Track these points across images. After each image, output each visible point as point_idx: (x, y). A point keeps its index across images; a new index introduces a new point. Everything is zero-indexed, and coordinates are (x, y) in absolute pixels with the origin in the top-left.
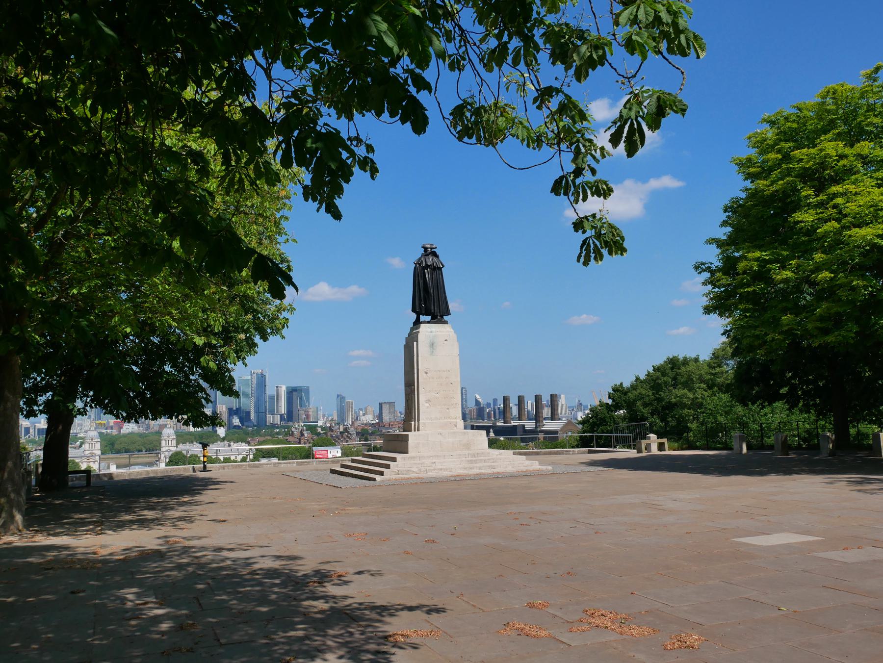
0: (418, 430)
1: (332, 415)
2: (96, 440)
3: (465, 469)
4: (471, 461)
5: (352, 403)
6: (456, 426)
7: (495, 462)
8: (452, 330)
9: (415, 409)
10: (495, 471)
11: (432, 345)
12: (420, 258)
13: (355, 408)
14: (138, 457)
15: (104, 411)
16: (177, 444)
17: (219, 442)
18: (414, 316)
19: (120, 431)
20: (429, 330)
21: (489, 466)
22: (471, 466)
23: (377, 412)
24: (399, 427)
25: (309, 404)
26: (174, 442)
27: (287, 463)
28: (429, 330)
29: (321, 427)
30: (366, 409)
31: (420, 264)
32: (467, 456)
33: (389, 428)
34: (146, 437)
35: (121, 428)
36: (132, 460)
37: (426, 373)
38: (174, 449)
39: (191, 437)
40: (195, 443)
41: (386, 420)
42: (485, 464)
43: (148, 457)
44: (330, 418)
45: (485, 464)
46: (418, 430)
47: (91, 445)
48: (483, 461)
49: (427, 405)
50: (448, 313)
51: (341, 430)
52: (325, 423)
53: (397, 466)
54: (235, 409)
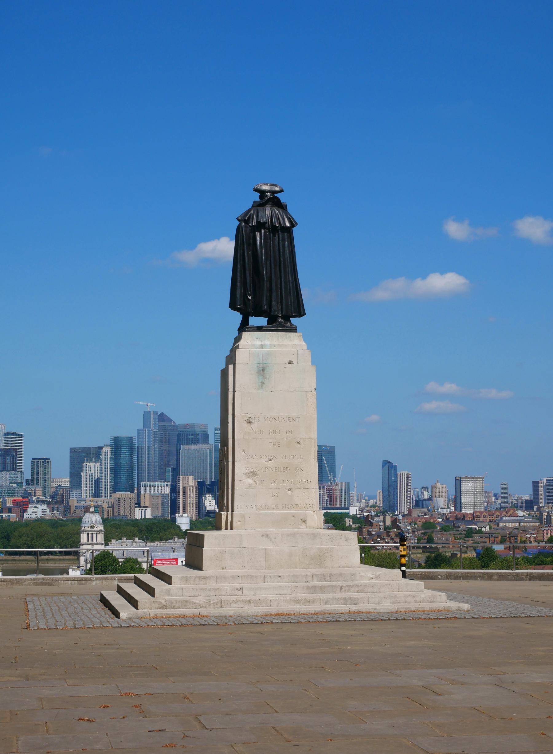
0: (232, 528)
1: (375, 497)
2: (98, 529)
3: (297, 602)
4: (314, 587)
5: (408, 478)
6: (304, 522)
7: (362, 591)
8: (304, 343)
9: (228, 489)
10: (354, 608)
11: (262, 371)
12: (249, 210)
13: (416, 485)
14: (47, 560)
15: (197, 486)
16: (107, 542)
17: (176, 539)
18: (238, 317)
19: (22, 516)
20: (258, 343)
21: (345, 599)
22: (310, 597)
23: (453, 493)
24: (490, 521)
25: (334, 477)
26: (101, 538)
27: (101, 579)
28: (258, 343)
29: (354, 517)
30: (434, 487)
31: (247, 222)
32: (310, 579)
33: (472, 522)
34: (61, 526)
35: (25, 510)
36: (42, 565)
37: (249, 422)
38: (103, 548)
39: (132, 529)
40: (136, 539)
41: (467, 508)
42: (338, 595)
43: (64, 560)
44: (371, 502)
45: (338, 595)
46: (232, 528)
47: (90, 535)
48: (339, 589)
49: (250, 481)
50: (300, 312)
51: (388, 523)
52: (361, 510)
53: (168, 592)
54: (208, 482)
